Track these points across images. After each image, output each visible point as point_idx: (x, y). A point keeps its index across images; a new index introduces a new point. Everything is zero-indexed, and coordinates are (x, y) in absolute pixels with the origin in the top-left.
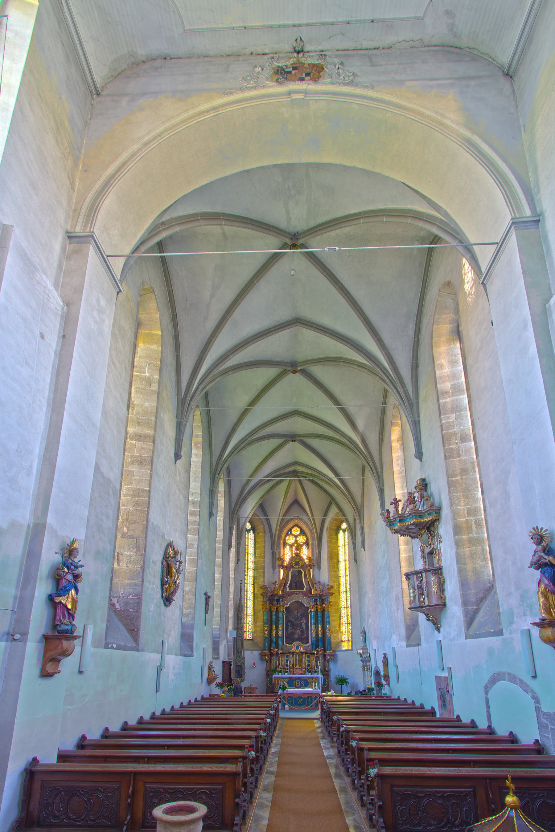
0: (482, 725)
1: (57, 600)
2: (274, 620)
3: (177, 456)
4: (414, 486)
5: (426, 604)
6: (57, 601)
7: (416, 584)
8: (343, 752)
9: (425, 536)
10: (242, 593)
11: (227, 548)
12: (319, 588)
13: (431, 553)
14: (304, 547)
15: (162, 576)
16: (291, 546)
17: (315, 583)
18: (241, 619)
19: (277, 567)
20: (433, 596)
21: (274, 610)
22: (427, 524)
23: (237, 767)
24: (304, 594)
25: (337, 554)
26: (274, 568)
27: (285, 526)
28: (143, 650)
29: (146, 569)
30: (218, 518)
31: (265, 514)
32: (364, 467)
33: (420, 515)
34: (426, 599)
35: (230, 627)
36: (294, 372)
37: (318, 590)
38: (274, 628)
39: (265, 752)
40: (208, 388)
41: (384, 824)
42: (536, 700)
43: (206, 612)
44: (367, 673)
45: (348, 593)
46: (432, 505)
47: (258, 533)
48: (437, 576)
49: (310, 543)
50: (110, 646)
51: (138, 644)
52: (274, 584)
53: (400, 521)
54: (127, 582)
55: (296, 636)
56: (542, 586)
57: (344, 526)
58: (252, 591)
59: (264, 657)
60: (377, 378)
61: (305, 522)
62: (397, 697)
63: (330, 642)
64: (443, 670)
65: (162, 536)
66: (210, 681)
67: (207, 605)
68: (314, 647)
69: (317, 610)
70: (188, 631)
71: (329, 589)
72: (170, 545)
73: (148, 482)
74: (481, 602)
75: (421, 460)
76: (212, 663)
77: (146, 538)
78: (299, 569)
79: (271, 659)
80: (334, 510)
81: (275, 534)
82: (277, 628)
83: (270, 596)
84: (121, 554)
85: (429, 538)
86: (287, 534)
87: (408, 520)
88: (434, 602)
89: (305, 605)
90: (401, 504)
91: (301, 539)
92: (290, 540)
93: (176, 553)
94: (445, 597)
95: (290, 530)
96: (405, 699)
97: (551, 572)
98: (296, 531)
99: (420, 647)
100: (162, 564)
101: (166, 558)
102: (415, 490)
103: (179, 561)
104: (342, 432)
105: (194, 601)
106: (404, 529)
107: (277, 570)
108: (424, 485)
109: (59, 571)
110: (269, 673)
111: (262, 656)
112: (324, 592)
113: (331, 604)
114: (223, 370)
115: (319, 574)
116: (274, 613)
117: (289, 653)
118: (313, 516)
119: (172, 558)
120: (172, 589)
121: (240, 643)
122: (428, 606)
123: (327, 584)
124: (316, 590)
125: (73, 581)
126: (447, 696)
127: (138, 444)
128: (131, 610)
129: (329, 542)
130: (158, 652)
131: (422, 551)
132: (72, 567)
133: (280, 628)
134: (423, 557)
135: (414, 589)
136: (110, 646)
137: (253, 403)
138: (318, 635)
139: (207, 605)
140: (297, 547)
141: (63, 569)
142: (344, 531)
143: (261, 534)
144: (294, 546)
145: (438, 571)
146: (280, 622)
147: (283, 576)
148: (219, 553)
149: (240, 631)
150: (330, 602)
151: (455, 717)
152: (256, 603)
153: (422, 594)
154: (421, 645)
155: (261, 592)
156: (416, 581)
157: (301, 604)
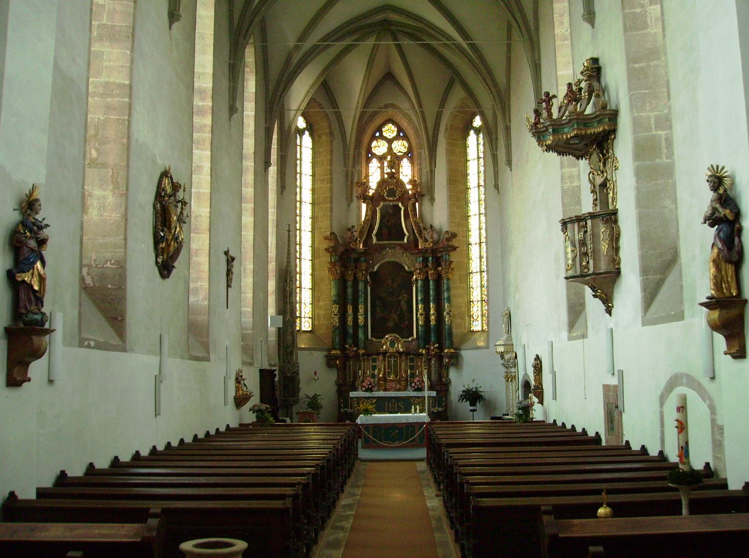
0: (673, 457)
1: (20, 277)
2: (350, 297)
3: (173, 16)
4: (580, 72)
6: (20, 279)
9: (595, 157)
10: (291, 248)
11: (262, 166)
12: (432, 237)
13: (604, 185)
14: (405, 160)
16: (381, 159)
17: (425, 229)
19: (355, 199)
20: (602, 258)
21: (350, 278)
24: (405, 248)
25: (466, 175)
27: (368, 127)
28: (133, 351)
29: (129, 218)
31: (334, 104)
34: (591, 262)
35: (272, 310)
37: (430, 240)
38: (350, 311)
42: (713, 410)
43: (228, 286)
44: (512, 386)
45: (484, 245)
46: (604, 107)
47: (320, 136)
48: (609, 225)
49: (415, 153)
50: (86, 343)
52: (349, 230)
55: (391, 324)
56: (716, 250)
57: (477, 122)
58: (310, 243)
59: (333, 362)
61: (406, 115)
62: (552, 422)
63: (450, 334)
64: (613, 374)
66: (240, 401)
67: (229, 272)
68: (422, 343)
69: (427, 277)
71: (449, 240)
73: (128, 71)
74: (667, 268)
75: (593, 27)
76: (241, 371)
77: (128, 166)
78: (395, 203)
80: (458, 95)
81: (350, 140)
82: (355, 311)
83: (342, 253)
84: (90, 195)
85: (600, 161)
86: (374, 138)
87: (566, 130)
88: (603, 268)
89: (406, 268)
90: (556, 103)
91: (400, 147)
92: (379, 148)
93: (176, 187)
94: (620, 259)
95: (379, 129)
96: (643, 447)
97: (727, 231)
98: (390, 131)
102: (582, 77)
107: (354, 205)
108: (595, 70)
109: (18, 235)
112: (441, 245)
113: (453, 265)
115: (432, 211)
116: (350, 284)
117: (378, 354)
118: (420, 106)
119: (170, 196)
120: (172, 249)
121: (289, 338)
122: (594, 274)
123: (445, 229)
124: (426, 240)
125: (37, 249)
126: (615, 413)
128: (110, 286)
129: (450, 152)
131: (592, 182)
132: (35, 228)
133: (361, 310)
134: (593, 192)
135: (574, 246)
136: (86, 343)
138: (430, 321)
139: (229, 272)
140: (390, 161)
141: (25, 233)
142: (477, 131)
143: (324, 138)
144: (389, 161)
145: (610, 217)
146: (361, 300)
147: (366, 215)
148: (249, 177)
149: (288, 317)
150: (451, 262)
152: (317, 266)
153: (586, 254)
157: (399, 267)
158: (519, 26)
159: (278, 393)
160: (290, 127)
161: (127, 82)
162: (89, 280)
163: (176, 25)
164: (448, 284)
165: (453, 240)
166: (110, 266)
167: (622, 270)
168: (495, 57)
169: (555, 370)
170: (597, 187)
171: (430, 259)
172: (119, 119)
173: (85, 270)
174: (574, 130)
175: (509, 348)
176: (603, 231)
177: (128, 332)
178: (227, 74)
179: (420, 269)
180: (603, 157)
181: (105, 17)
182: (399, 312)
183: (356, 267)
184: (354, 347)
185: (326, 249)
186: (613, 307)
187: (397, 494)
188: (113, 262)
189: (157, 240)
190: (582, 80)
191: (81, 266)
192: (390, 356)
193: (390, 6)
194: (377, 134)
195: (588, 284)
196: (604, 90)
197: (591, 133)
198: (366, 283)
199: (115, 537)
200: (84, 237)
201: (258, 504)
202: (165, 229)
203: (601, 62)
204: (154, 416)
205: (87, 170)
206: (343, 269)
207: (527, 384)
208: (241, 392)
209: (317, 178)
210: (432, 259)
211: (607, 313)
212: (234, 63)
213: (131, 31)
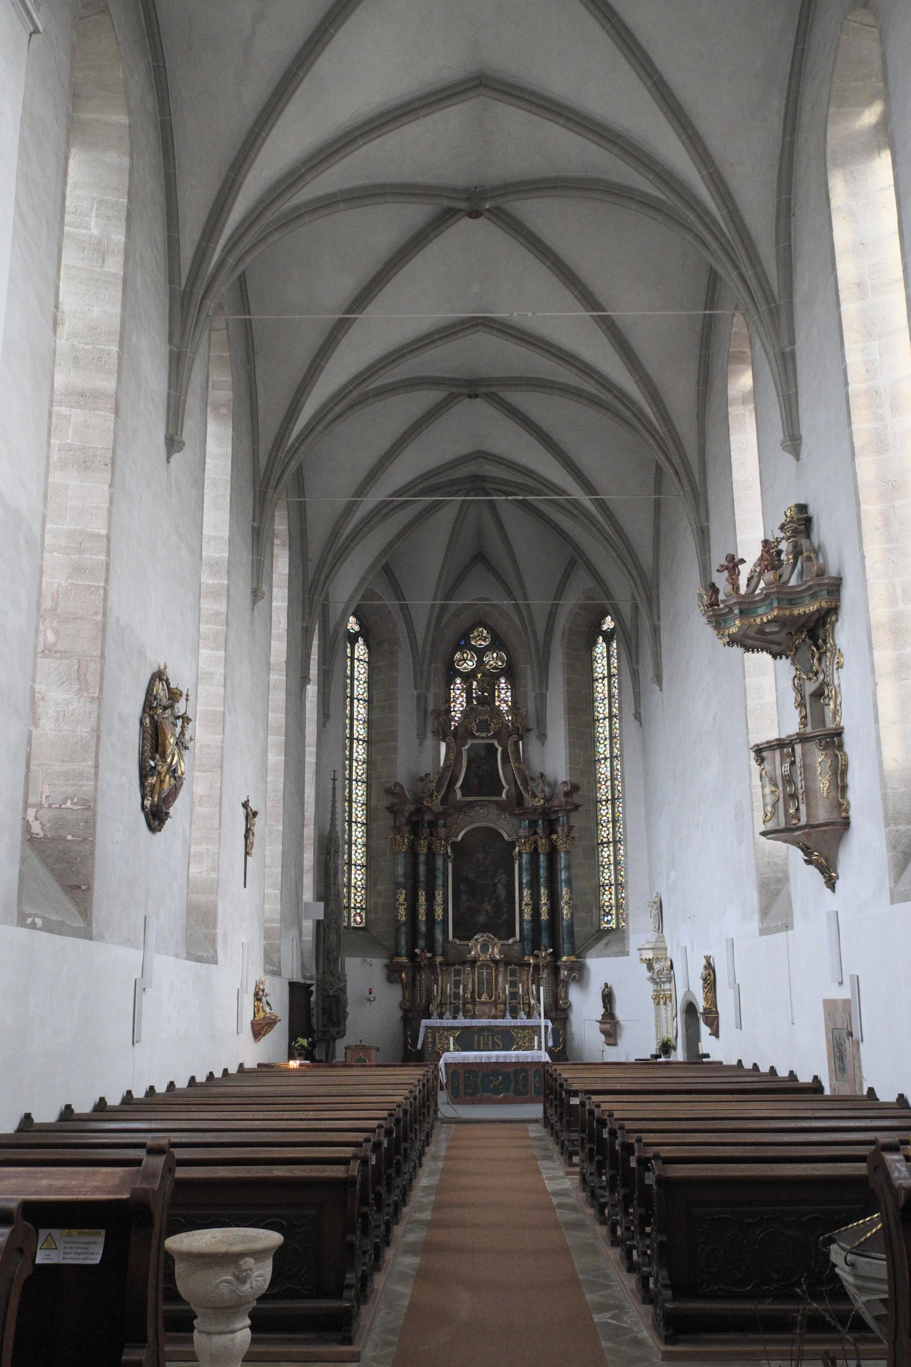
2: (422, 878)
3: (173, 444)
4: (779, 524)
5: (803, 821)
7: (778, 772)
8: (591, 1174)
9: (804, 652)
12: (543, 791)
13: (819, 694)
15: (142, 753)
16: (468, 677)
17: (532, 779)
18: (336, 874)
19: (430, 735)
20: (821, 802)
22: (808, 620)
23: (347, 1171)
26: (422, 736)
28: (101, 938)
29: (104, 736)
30: (274, 604)
32: (659, 470)
33: (790, 598)
34: (803, 808)
35: (308, 895)
36: (475, 214)
38: (422, 899)
39: (407, 1177)
40: (248, 260)
41: (670, 1279)
43: (247, 854)
44: (666, 1012)
46: (821, 573)
48: (829, 752)
50: (29, 920)
51: (89, 924)
52: (422, 779)
53: (741, 612)
54: (57, 767)
55: (482, 919)
57: (608, 624)
59: (395, 976)
60: (689, 238)
63: (571, 934)
64: (841, 983)
65: (140, 653)
66: (260, 1029)
68: (528, 947)
69: (536, 849)
70: (203, 899)
71: (567, 794)
72: (159, 676)
75: (798, 459)
76: (263, 983)
79: (414, 979)
80: (581, 582)
82: (431, 898)
83: (412, 814)
87: (761, 611)
88: (822, 815)
89: (505, 836)
90: (745, 571)
93: (174, 695)
94: (848, 803)
99: (790, 932)
100: (141, 723)
101: (151, 708)
102: (782, 535)
103: (182, 717)
104: (602, 376)
105: (216, 822)
106: (752, 632)
107: (430, 741)
108: (802, 522)
110: (410, 1015)
111: (392, 973)
112: (556, 802)
113: (574, 833)
114: (286, 210)
116: (422, 858)
117: (463, 963)
120: (166, 786)
121: (333, 937)
122: (809, 826)
124: (534, 796)
126: (847, 1045)
127: (77, 415)
128: (69, 837)
129: (570, 668)
130: (134, 945)
131: (799, 690)
133: (439, 899)
134: (801, 705)
135: (776, 785)
136: (29, 920)
137: (362, 299)
138: (539, 915)
142: (609, 637)
146: (440, 882)
149: (333, 905)
151: (865, 1093)
153: (794, 796)
154: (792, 928)
155: (387, 803)
156: (776, 763)
158: (677, 473)
159: (314, 1020)
160: (336, 631)
161: (104, 532)
162: (36, 828)
163: (176, 457)
164: (567, 860)
165: (575, 795)
166: (71, 806)
167: (854, 821)
168: (637, 526)
169: (737, 982)
170: (807, 697)
171: (540, 822)
172: (91, 586)
173: (31, 813)
174: (772, 610)
175: (660, 954)
176: (820, 760)
177: (95, 909)
178: (249, 540)
179: (525, 837)
180: (818, 649)
181: (70, 435)
182: (494, 901)
183: (432, 835)
184: (429, 951)
185: (387, 808)
186: (837, 878)
187: (499, 1175)
188: (75, 800)
189: (144, 773)
190: (782, 539)
191: (26, 805)
192: (481, 967)
193: (485, 453)
194: (463, 643)
195: (797, 844)
196: (817, 551)
197: (799, 614)
198: (446, 857)
199: (79, 1193)
200: (32, 762)
201: (303, 1171)
202: (158, 756)
203: (812, 511)
204: (131, 1042)
205: (39, 660)
206: (412, 837)
207: (690, 1009)
208: (262, 1015)
209: (375, 704)
210: (543, 823)
211: (829, 887)
212: (259, 527)
213: (111, 455)
